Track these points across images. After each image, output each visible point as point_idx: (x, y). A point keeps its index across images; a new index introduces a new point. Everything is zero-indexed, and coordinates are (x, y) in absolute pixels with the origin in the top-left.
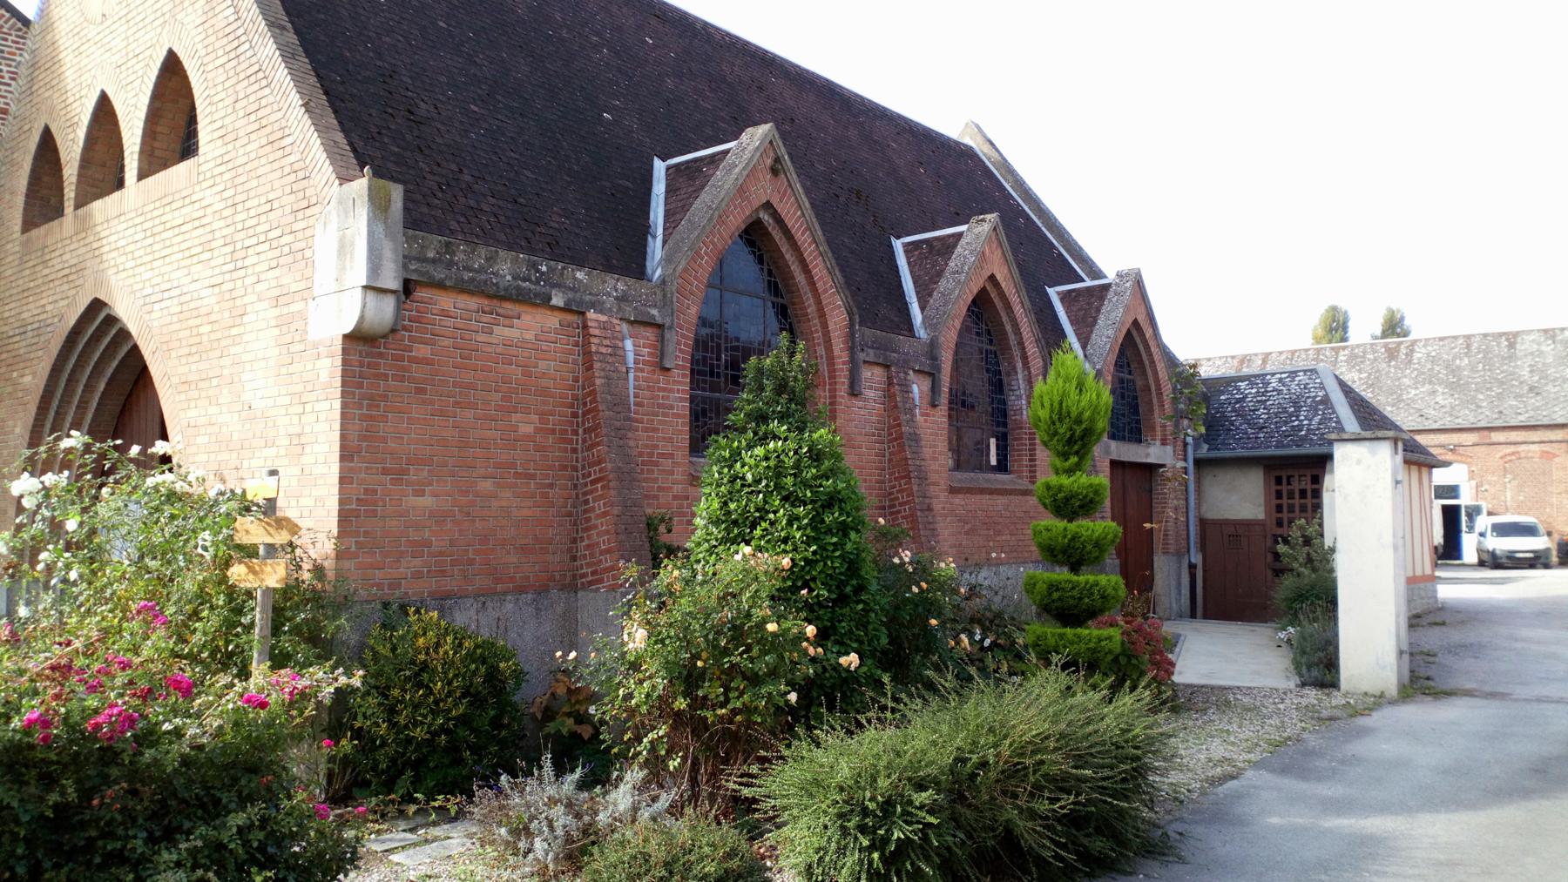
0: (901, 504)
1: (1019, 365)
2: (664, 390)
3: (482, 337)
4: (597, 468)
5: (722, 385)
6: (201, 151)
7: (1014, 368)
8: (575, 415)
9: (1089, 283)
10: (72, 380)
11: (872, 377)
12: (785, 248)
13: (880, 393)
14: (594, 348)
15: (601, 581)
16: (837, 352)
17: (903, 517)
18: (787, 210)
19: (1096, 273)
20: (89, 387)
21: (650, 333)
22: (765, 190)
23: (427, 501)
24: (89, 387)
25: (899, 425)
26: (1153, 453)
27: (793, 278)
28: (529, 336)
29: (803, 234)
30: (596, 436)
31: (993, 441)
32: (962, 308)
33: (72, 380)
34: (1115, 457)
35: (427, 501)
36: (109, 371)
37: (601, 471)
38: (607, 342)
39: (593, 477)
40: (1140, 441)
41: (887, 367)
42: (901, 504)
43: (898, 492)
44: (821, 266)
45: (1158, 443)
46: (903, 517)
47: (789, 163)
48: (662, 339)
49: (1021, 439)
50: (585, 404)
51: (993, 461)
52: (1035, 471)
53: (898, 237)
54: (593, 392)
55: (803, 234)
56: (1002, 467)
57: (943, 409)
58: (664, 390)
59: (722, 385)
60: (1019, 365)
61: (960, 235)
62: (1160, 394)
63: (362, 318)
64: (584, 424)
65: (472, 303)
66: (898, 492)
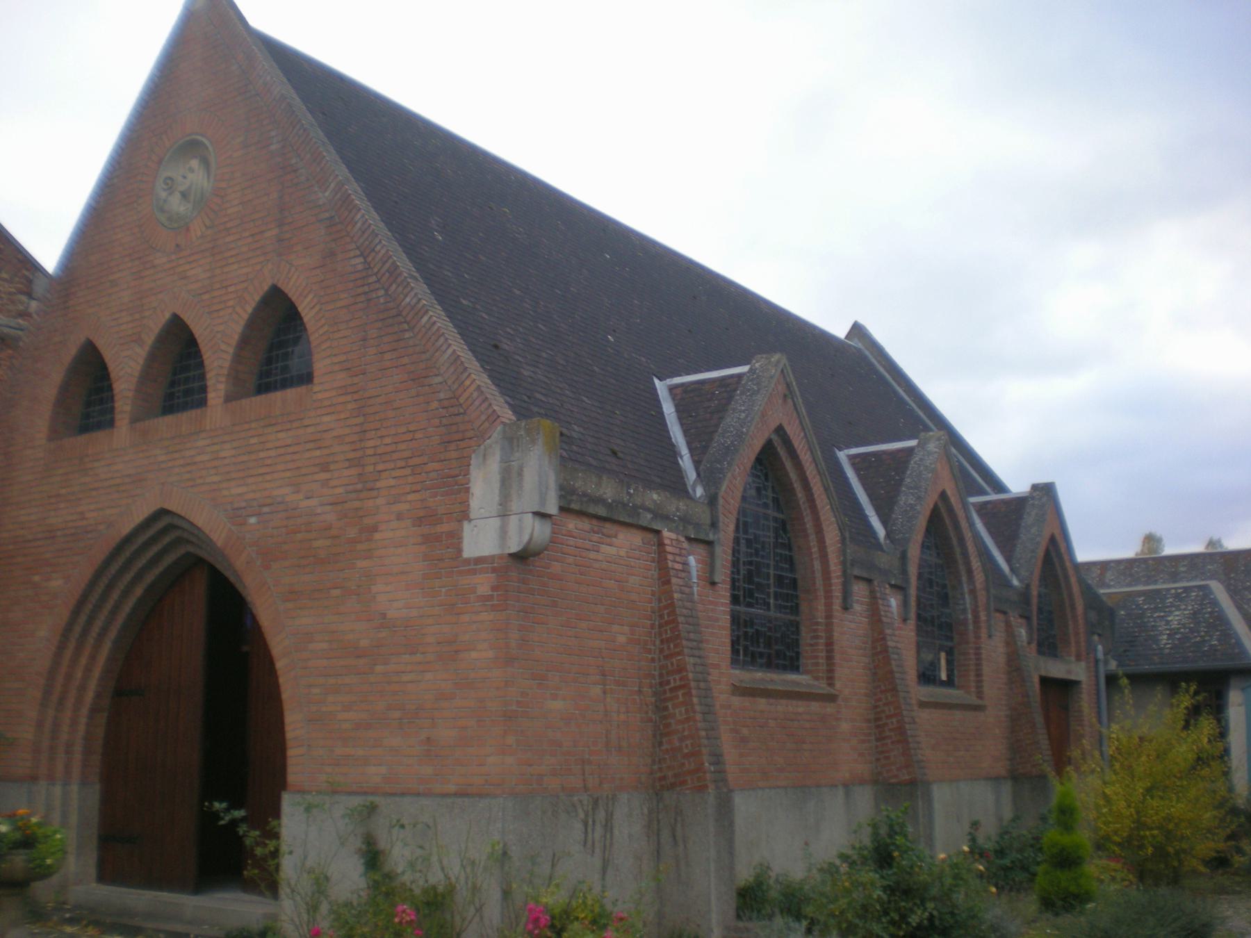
0: (888, 717)
1: (964, 579)
2: (711, 603)
3: (592, 555)
4: (677, 677)
5: (742, 598)
6: (316, 381)
7: (960, 582)
8: (652, 626)
9: (993, 497)
10: (109, 587)
11: (859, 589)
12: (788, 465)
13: (865, 607)
14: (670, 564)
15: (684, 783)
16: (833, 568)
17: (890, 730)
18: (793, 431)
19: (998, 486)
20: (126, 593)
21: (701, 549)
22: (780, 415)
23: (558, 705)
24: (126, 593)
25: (884, 639)
26: (1077, 671)
27: (795, 495)
28: (622, 553)
29: (805, 454)
30: (676, 646)
31: (943, 655)
32: (921, 522)
33: (109, 587)
34: (1043, 674)
35: (558, 705)
36: (150, 578)
37: (681, 679)
38: (678, 559)
39: (672, 685)
40: (732, 663)
41: (869, 581)
42: (888, 717)
43: (885, 704)
44: (819, 484)
45: (1073, 658)
46: (890, 730)
47: (796, 388)
48: (712, 555)
49: (817, 657)
50: (661, 616)
51: (944, 677)
52: (982, 687)
53: (840, 450)
54: (672, 605)
55: (805, 454)
56: (950, 683)
57: (912, 623)
58: (711, 603)
59: (742, 598)
60: (964, 579)
61: (910, 451)
62: (1073, 607)
63: (531, 539)
64: (660, 634)
65: (585, 524)
66: (885, 704)
